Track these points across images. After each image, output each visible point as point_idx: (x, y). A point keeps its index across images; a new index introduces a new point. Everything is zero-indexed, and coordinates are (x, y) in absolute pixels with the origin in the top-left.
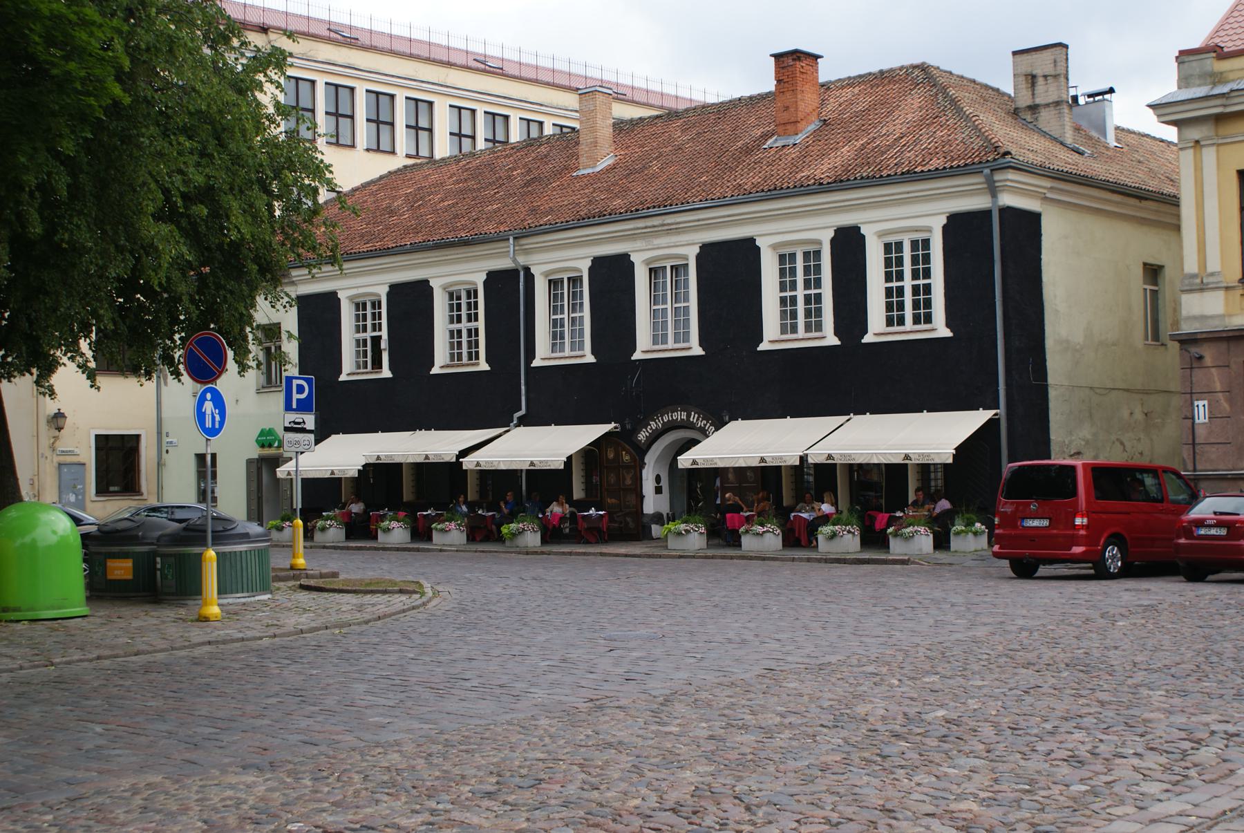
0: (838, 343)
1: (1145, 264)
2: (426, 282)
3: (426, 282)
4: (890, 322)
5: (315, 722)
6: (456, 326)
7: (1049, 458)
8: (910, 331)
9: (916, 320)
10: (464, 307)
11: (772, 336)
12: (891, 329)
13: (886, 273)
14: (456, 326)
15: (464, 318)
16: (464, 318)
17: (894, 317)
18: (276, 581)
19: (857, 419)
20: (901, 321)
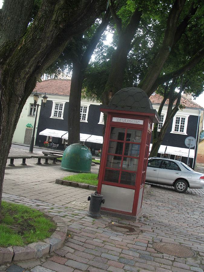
0: (63, 119)
1: (30, 103)
2: (52, 101)
3: (52, 101)
4: (54, 116)
5: (181, 163)
6: (56, 110)
7: (193, 159)
8: (57, 118)
9: (59, 116)
10: (59, 107)
11: (173, 131)
12: (175, 132)
13: (176, 120)
14: (56, 110)
15: (59, 109)
16: (59, 109)
17: (176, 129)
18: (118, 145)
19: (93, 136)
20: (56, 116)
